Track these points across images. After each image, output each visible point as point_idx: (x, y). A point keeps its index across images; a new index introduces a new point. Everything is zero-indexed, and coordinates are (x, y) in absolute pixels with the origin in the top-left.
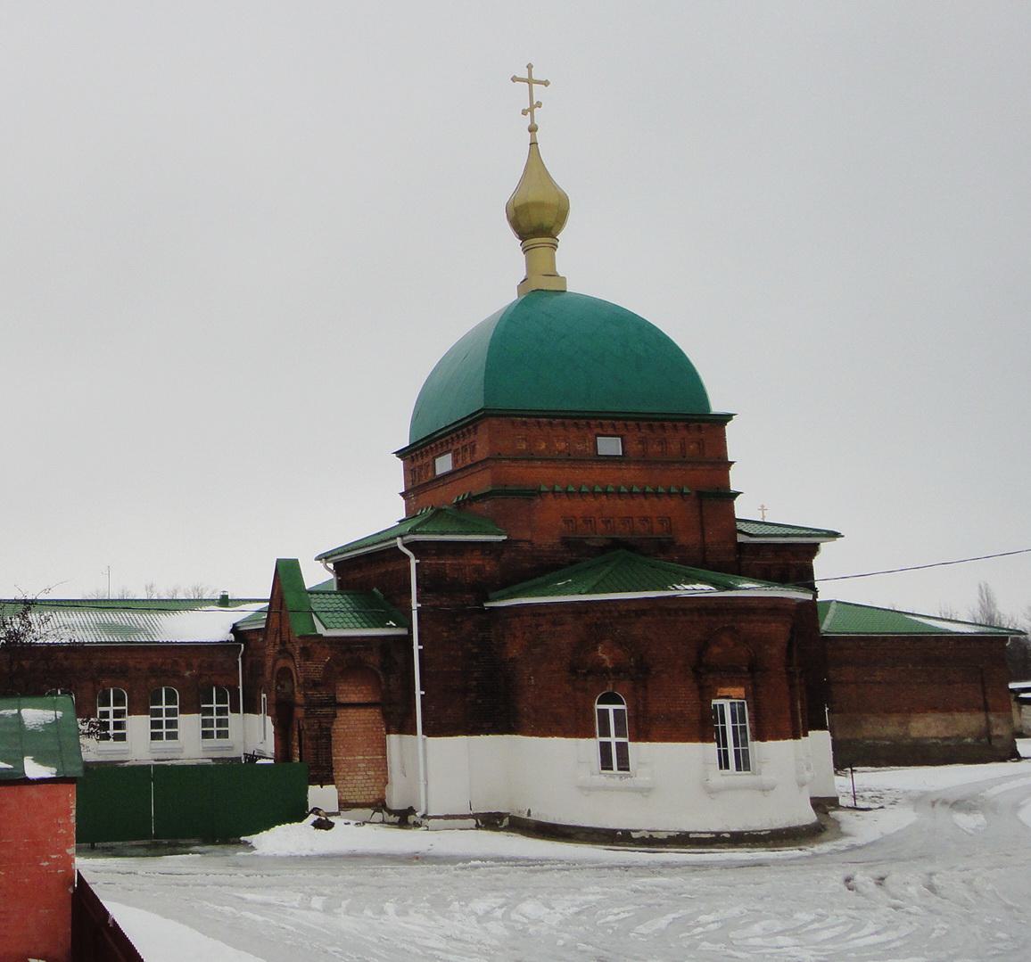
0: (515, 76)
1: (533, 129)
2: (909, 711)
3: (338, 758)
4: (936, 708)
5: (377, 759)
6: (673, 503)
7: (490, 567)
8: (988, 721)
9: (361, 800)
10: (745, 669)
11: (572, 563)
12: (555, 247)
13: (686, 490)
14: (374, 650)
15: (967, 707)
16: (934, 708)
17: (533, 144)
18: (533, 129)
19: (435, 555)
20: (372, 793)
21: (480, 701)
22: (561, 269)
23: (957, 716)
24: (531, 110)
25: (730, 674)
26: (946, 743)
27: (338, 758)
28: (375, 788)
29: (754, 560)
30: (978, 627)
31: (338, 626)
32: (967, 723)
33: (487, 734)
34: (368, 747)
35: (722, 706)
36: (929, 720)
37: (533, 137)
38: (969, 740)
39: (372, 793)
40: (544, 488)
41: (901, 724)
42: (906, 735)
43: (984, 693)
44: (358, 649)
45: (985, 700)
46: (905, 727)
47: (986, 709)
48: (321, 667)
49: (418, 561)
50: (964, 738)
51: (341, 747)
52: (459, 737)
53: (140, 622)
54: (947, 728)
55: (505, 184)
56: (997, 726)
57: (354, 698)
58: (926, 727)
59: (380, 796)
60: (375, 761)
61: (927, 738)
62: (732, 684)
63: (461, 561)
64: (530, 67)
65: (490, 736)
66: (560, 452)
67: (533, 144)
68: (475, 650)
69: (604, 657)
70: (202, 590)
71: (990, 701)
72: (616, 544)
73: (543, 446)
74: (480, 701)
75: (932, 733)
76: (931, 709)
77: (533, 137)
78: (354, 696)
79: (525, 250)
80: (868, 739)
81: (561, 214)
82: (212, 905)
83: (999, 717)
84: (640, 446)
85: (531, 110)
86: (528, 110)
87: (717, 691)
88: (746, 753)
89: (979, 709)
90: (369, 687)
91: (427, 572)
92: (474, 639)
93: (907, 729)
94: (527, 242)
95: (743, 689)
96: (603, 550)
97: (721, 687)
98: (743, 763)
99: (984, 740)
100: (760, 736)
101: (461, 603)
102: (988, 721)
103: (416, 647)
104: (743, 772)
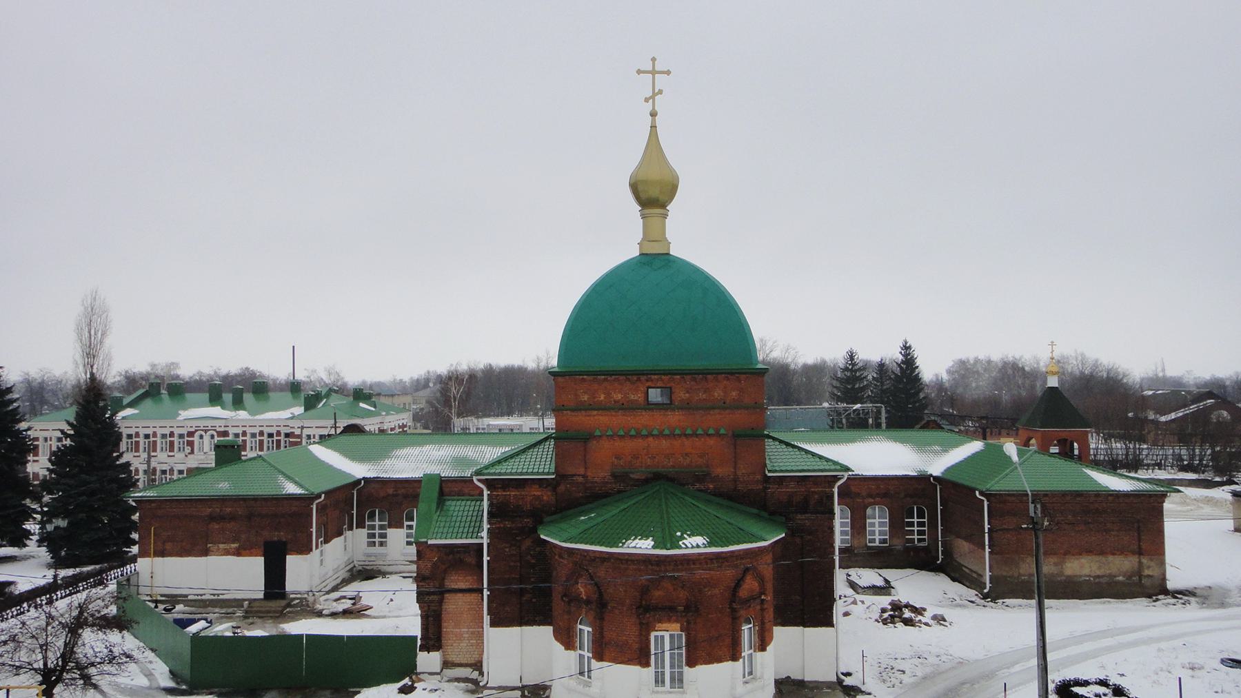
0: (639, 70)
1: (653, 114)
2: (1065, 554)
3: (448, 630)
4: (1090, 552)
5: (478, 632)
6: (711, 442)
7: (547, 496)
8: (1140, 563)
9: (464, 661)
10: (682, 608)
11: (619, 492)
12: (665, 216)
13: (722, 431)
14: (472, 553)
15: (1121, 551)
16: (1089, 552)
17: (653, 127)
18: (653, 114)
19: (500, 488)
20: (474, 656)
21: (534, 600)
22: (669, 235)
23: (1111, 558)
24: (653, 97)
25: (667, 611)
26: (1097, 580)
27: (448, 630)
28: (476, 653)
29: (778, 488)
30: (1136, 483)
31: (479, 518)
32: (1120, 565)
33: (539, 625)
34: (472, 622)
35: (663, 637)
36: (1083, 560)
37: (654, 121)
38: (1121, 578)
39: (474, 656)
40: (598, 433)
41: (1056, 564)
42: (1061, 574)
43: (1140, 541)
44: (458, 552)
45: (1139, 545)
46: (1060, 567)
47: (1140, 553)
48: (429, 565)
49: (489, 492)
50: (1115, 576)
51: (451, 621)
52: (515, 628)
53: (487, 455)
54: (1099, 568)
55: (630, 159)
56: (1149, 567)
57: (462, 585)
58: (1081, 567)
59: (480, 659)
60: (476, 633)
61: (1081, 576)
62: (669, 621)
63: (523, 493)
64: (654, 60)
65: (541, 627)
66: (615, 402)
67: (653, 127)
68: (533, 561)
69: (582, 590)
70: (765, 341)
71: (1143, 547)
72: (657, 477)
73: (602, 397)
74: (534, 600)
75: (1086, 571)
76: (1087, 552)
77: (654, 121)
78: (462, 584)
79: (643, 217)
80: (1023, 576)
81: (671, 189)
82: (1116, 432)
83: (1152, 560)
84: (687, 395)
85: (653, 97)
86: (657, 94)
87: (655, 626)
88: (681, 674)
89: (1133, 553)
90: (475, 578)
91: (495, 501)
92: (532, 553)
93: (1062, 568)
94: (647, 211)
95: (679, 625)
96: (646, 481)
97: (659, 623)
98: (678, 681)
99: (1135, 579)
100: (691, 663)
101: (521, 525)
102: (1140, 563)
103: (486, 558)
104: (676, 690)
